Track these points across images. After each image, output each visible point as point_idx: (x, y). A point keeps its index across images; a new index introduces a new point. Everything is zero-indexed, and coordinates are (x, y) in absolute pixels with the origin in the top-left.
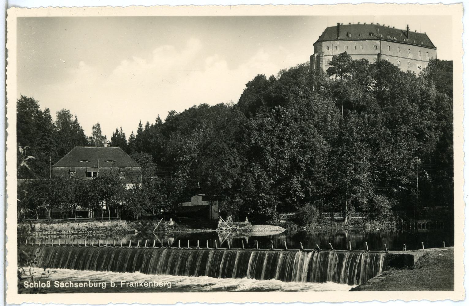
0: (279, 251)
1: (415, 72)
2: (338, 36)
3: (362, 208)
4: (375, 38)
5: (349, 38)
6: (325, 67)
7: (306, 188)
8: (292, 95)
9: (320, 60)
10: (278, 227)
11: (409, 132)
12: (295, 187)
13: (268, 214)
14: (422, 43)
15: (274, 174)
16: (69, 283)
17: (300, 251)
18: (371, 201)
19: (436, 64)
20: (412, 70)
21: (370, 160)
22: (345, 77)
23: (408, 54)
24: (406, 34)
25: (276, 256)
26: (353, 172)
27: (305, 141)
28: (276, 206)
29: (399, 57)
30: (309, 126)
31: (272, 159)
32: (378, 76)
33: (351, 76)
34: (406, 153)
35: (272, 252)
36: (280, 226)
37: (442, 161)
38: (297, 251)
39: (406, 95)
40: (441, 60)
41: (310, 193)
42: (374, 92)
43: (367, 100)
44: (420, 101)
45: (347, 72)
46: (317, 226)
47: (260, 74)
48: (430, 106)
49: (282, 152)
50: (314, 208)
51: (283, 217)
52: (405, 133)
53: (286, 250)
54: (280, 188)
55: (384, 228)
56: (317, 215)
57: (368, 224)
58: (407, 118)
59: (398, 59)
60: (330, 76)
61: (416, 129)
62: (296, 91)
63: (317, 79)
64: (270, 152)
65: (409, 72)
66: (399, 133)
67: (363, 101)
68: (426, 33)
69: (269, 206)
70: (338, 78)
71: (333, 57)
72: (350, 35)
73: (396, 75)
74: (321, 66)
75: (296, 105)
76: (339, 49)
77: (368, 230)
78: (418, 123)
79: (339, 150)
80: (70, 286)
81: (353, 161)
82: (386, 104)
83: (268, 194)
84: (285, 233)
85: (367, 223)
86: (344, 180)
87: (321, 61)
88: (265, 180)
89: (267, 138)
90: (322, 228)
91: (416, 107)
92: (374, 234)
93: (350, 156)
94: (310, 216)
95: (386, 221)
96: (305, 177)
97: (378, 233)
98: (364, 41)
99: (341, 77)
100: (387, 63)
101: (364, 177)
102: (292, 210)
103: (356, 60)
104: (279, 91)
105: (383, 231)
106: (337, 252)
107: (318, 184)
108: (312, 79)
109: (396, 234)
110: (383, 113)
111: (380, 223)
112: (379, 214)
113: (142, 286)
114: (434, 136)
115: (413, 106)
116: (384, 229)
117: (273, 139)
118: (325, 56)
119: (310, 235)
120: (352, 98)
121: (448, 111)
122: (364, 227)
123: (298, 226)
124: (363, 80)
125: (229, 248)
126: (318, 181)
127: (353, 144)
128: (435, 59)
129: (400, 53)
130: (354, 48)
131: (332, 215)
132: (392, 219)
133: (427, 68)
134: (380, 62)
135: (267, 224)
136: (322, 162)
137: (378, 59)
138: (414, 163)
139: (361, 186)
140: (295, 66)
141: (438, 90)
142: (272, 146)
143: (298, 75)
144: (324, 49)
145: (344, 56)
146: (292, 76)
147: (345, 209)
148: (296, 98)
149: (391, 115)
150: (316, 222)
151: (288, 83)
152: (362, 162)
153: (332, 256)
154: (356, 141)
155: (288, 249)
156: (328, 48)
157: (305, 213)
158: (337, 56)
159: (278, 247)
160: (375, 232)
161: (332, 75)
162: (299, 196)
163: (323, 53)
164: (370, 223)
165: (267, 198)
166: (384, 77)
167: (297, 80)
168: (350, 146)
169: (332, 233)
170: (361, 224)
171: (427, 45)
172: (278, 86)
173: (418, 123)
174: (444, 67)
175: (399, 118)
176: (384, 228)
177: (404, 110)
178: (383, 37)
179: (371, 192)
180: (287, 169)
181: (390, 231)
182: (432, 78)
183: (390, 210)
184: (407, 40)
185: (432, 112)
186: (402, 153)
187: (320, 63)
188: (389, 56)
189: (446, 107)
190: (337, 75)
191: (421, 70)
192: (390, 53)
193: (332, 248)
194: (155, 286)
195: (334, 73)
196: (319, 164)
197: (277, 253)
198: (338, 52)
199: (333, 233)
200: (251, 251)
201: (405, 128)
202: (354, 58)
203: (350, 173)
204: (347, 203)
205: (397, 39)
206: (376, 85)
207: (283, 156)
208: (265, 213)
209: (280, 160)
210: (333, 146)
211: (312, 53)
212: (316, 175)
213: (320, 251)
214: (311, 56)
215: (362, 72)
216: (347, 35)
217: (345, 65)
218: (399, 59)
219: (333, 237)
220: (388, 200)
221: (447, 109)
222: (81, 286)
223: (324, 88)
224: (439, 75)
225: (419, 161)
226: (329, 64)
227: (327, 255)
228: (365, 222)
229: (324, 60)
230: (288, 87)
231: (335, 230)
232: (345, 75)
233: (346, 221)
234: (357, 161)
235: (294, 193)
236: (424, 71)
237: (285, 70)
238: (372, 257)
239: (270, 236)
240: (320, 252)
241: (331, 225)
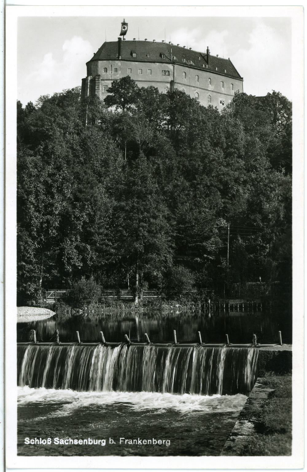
0: (68, 345)
2: (119, 55)
4: (167, 60)
5: (134, 58)
6: (102, 95)
8: (58, 129)
10: (45, 309)
11: (212, 185)
12: (68, 254)
13: (30, 291)
14: (225, 72)
15: (39, 236)
16: (35, 440)
17: (100, 346)
18: (167, 275)
19: (243, 99)
20: (214, 105)
21: (168, 219)
22: (129, 109)
23: (208, 85)
24: (206, 57)
25: (65, 353)
27: (80, 191)
28: (41, 281)
29: (197, 87)
30: (85, 171)
31: (37, 214)
32: (171, 111)
34: (208, 212)
35: (57, 347)
36: (46, 307)
37: (255, 224)
38: (96, 345)
39: (208, 137)
40: (249, 95)
41: (89, 262)
42: (167, 131)
43: (159, 142)
44: (225, 145)
46: (98, 307)
48: (237, 152)
49: (52, 205)
51: (52, 296)
52: (206, 185)
53: (79, 345)
54: (46, 256)
55: (185, 311)
57: (165, 306)
58: (209, 166)
59: (195, 91)
60: (108, 107)
61: (220, 181)
63: (91, 110)
64: (33, 204)
65: (210, 107)
66: (199, 186)
67: (153, 141)
68: (230, 59)
70: (120, 110)
72: (134, 55)
73: (195, 111)
74: (96, 93)
76: (120, 72)
77: (165, 313)
80: (70, 443)
81: (146, 220)
82: (181, 148)
84: (54, 318)
85: (163, 304)
86: (135, 245)
87: (96, 87)
90: (105, 311)
92: (173, 319)
93: (142, 213)
94: (88, 294)
95: (188, 301)
96: (82, 241)
97: (179, 317)
98: (152, 63)
99: (124, 110)
100: (182, 94)
101: (162, 240)
103: (143, 88)
104: (40, 123)
105: (185, 315)
106: (156, 346)
108: (85, 110)
109: (202, 318)
110: (178, 159)
111: (181, 304)
112: (180, 292)
113: (141, 444)
114: (241, 191)
115: (216, 151)
116: (187, 312)
117: (39, 187)
118: (102, 80)
119: (89, 320)
120: (138, 138)
121: (259, 160)
122: (160, 310)
124: (152, 115)
126: (99, 247)
127: (146, 197)
128: (242, 93)
129: (198, 83)
130: (139, 71)
131: (118, 293)
132: (196, 299)
134: (173, 92)
135: (28, 306)
136: (105, 221)
137: (171, 89)
138: (217, 225)
139: (156, 254)
140: (61, 91)
142: (37, 196)
143: (65, 103)
144: (101, 72)
145: (126, 81)
146: (58, 105)
147: (135, 284)
148: (65, 134)
150: (96, 303)
151: (53, 113)
152: (158, 221)
153: (149, 352)
155: (82, 343)
156: (106, 70)
157: (81, 290)
158: (118, 81)
159: (43, 339)
160: (174, 316)
161: (111, 105)
162: (74, 265)
163: (99, 76)
164: (168, 304)
166: (180, 112)
167: (64, 110)
168: (142, 199)
169: (118, 317)
170: (155, 305)
171: (231, 74)
172: (39, 117)
173: (223, 174)
174: (253, 104)
175: (199, 166)
177: (206, 157)
178: (177, 60)
181: (193, 315)
182: (238, 116)
183: (194, 286)
184: (207, 66)
185: (240, 160)
186: (203, 212)
187: (95, 90)
188: (185, 85)
189: (258, 155)
190: (117, 106)
191: (225, 106)
192: (185, 81)
193: (149, 341)
194: (153, 444)
195: (114, 104)
197: (66, 349)
198: (119, 76)
199: (119, 318)
200: (25, 346)
201: (207, 180)
202: (140, 85)
203: (143, 235)
204: (137, 276)
206: (169, 122)
207: (52, 210)
209: (49, 217)
211: (85, 75)
212: (97, 238)
213: (131, 345)
214: (83, 80)
215: (150, 104)
216: (131, 54)
217: (128, 93)
218: (198, 90)
219: (119, 322)
220: (191, 273)
221: (259, 157)
222: (160, 443)
224: (246, 114)
225: (223, 222)
226: (107, 91)
227: (141, 351)
228: (161, 302)
229: (100, 86)
230: (53, 119)
231: (121, 313)
232: (128, 107)
233: (137, 301)
234: (152, 220)
235: (67, 261)
237: (47, 97)
238: (138, 348)
239: (33, 322)
240: (130, 347)
241: (117, 307)
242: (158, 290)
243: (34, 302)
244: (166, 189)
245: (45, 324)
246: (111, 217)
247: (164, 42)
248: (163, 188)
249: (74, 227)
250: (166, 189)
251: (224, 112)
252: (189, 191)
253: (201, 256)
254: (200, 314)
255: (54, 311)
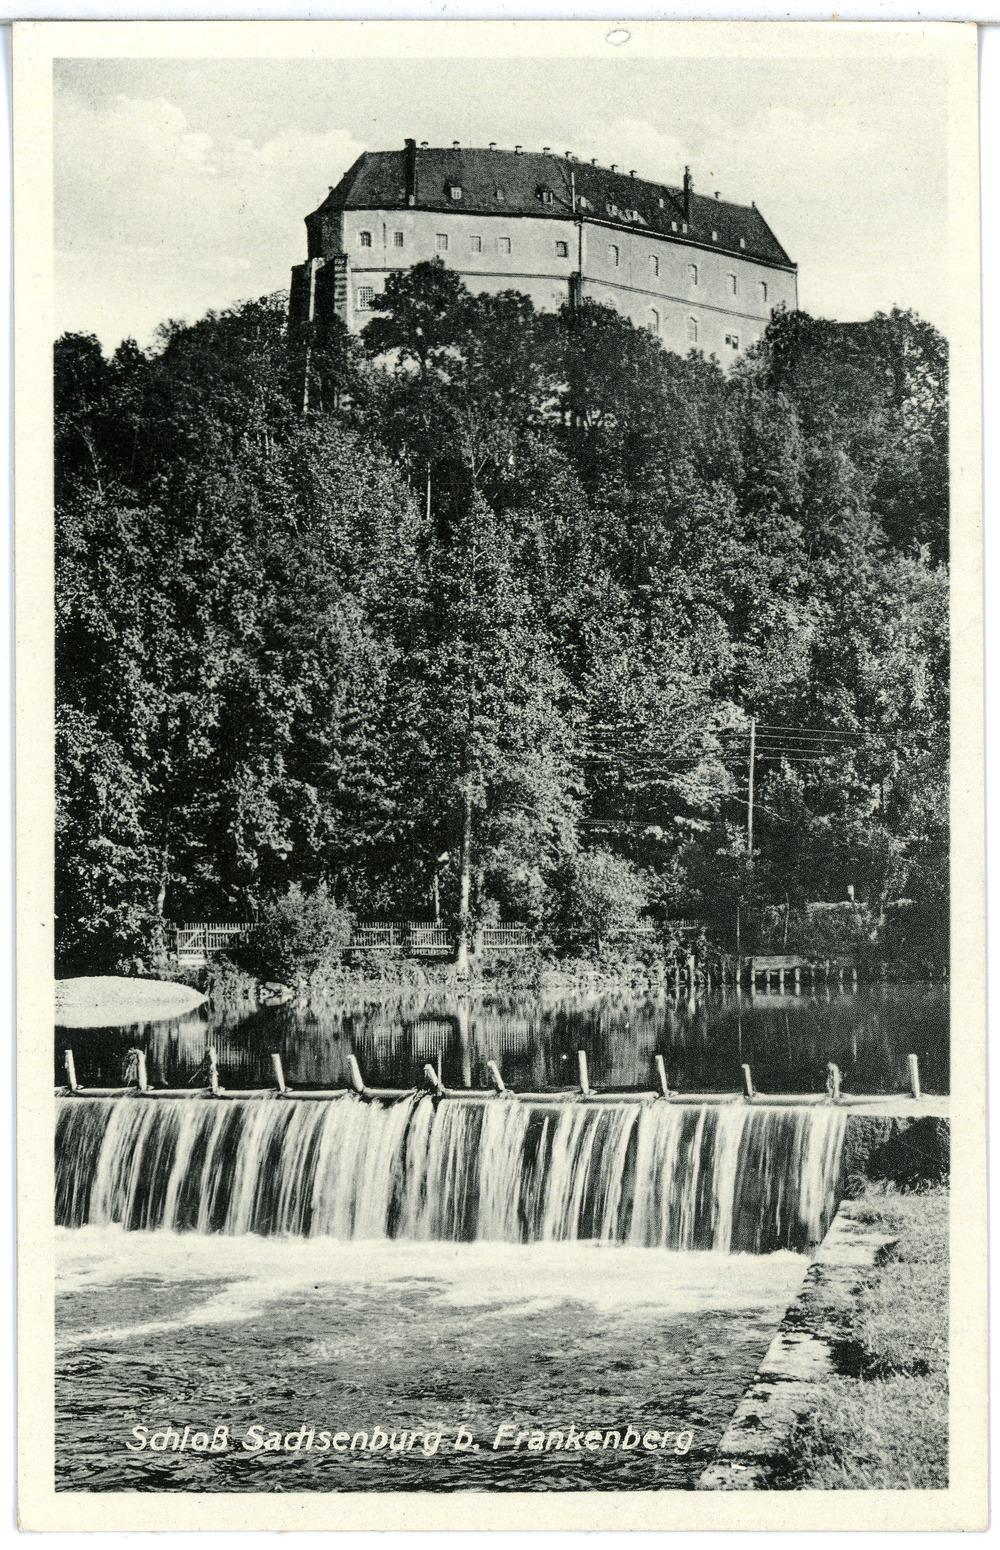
1: (717, 357)
3: (528, 908)
6: (356, 317)
7: (296, 819)
9: (332, 288)
11: (699, 599)
12: (247, 813)
18: (560, 880)
22: (439, 361)
24: (681, 203)
26: (493, 751)
27: (285, 616)
29: (654, 294)
33: (464, 359)
36: (179, 980)
41: (312, 840)
45: (447, 343)
47: (74, 330)
49: (197, 659)
50: (327, 906)
55: (616, 993)
56: (342, 934)
58: (692, 539)
60: (374, 355)
61: (725, 585)
62: (235, 408)
63: (319, 365)
64: (138, 657)
65: (695, 354)
66: (659, 603)
69: (128, 892)
70: (412, 365)
71: (387, 275)
72: (456, 193)
74: (336, 311)
75: (234, 468)
78: (735, 565)
79: (434, 658)
83: (128, 840)
84: (203, 1013)
87: (338, 290)
88: (115, 778)
89: (126, 599)
91: (729, 501)
93: (480, 686)
94: (310, 939)
96: (291, 773)
102: (240, 913)
103: (484, 296)
105: (615, 1005)
107: (343, 801)
109: (667, 1016)
112: (598, 931)
114: (792, 618)
115: (712, 491)
117: (156, 602)
118: (355, 270)
119: (311, 1020)
123: (258, 984)
125: (70, 1087)
127: (493, 634)
133: (761, 346)
134: (579, 306)
135: (121, 974)
136: (364, 710)
137: (572, 296)
138: (717, 723)
141: (807, 437)
142: (149, 629)
144: (350, 242)
145: (431, 277)
147: (457, 907)
149: (629, 525)
154: (507, 625)
157: (287, 928)
158: (406, 273)
165: (123, 858)
169: (403, 1009)
173: (735, 565)
174: (828, 343)
175: (659, 538)
176: (616, 993)
179: (569, 843)
180: (212, 734)
181: (641, 1003)
183: (643, 913)
184: (685, 226)
189: (844, 504)
190: (403, 352)
191: (741, 352)
196: (344, 719)
198: (406, 260)
199: (408, 1016)
201: (685, 584)
202: (475, 288)
205: (646, 219)
206: (567, 403)
207: (198, 676)
208: (116, 925)
210: (406, 645)
211: (300, 256)
213: (444, 1096)
216: (447, 191)
219: (407, 1026)
223: (353, 404)
225: (734, 716)
227: (475, 1116)
229: (349, 289)
232: (437, 353)
234: (511, 708)
236: (751, 356)
240: (443, 1103)
242: (530, 926)
243: (140, 962)
244: (555, 610)
245: (174, 1034)
246: (383, 698)
247: (550, 152)
248: (547, 606)
249: (266, 728)
250: (555, 610)
251: (737, 370)
252: (628, 616)
253: (665, 822)
254: (660, 1004)
255: (202, 990)
